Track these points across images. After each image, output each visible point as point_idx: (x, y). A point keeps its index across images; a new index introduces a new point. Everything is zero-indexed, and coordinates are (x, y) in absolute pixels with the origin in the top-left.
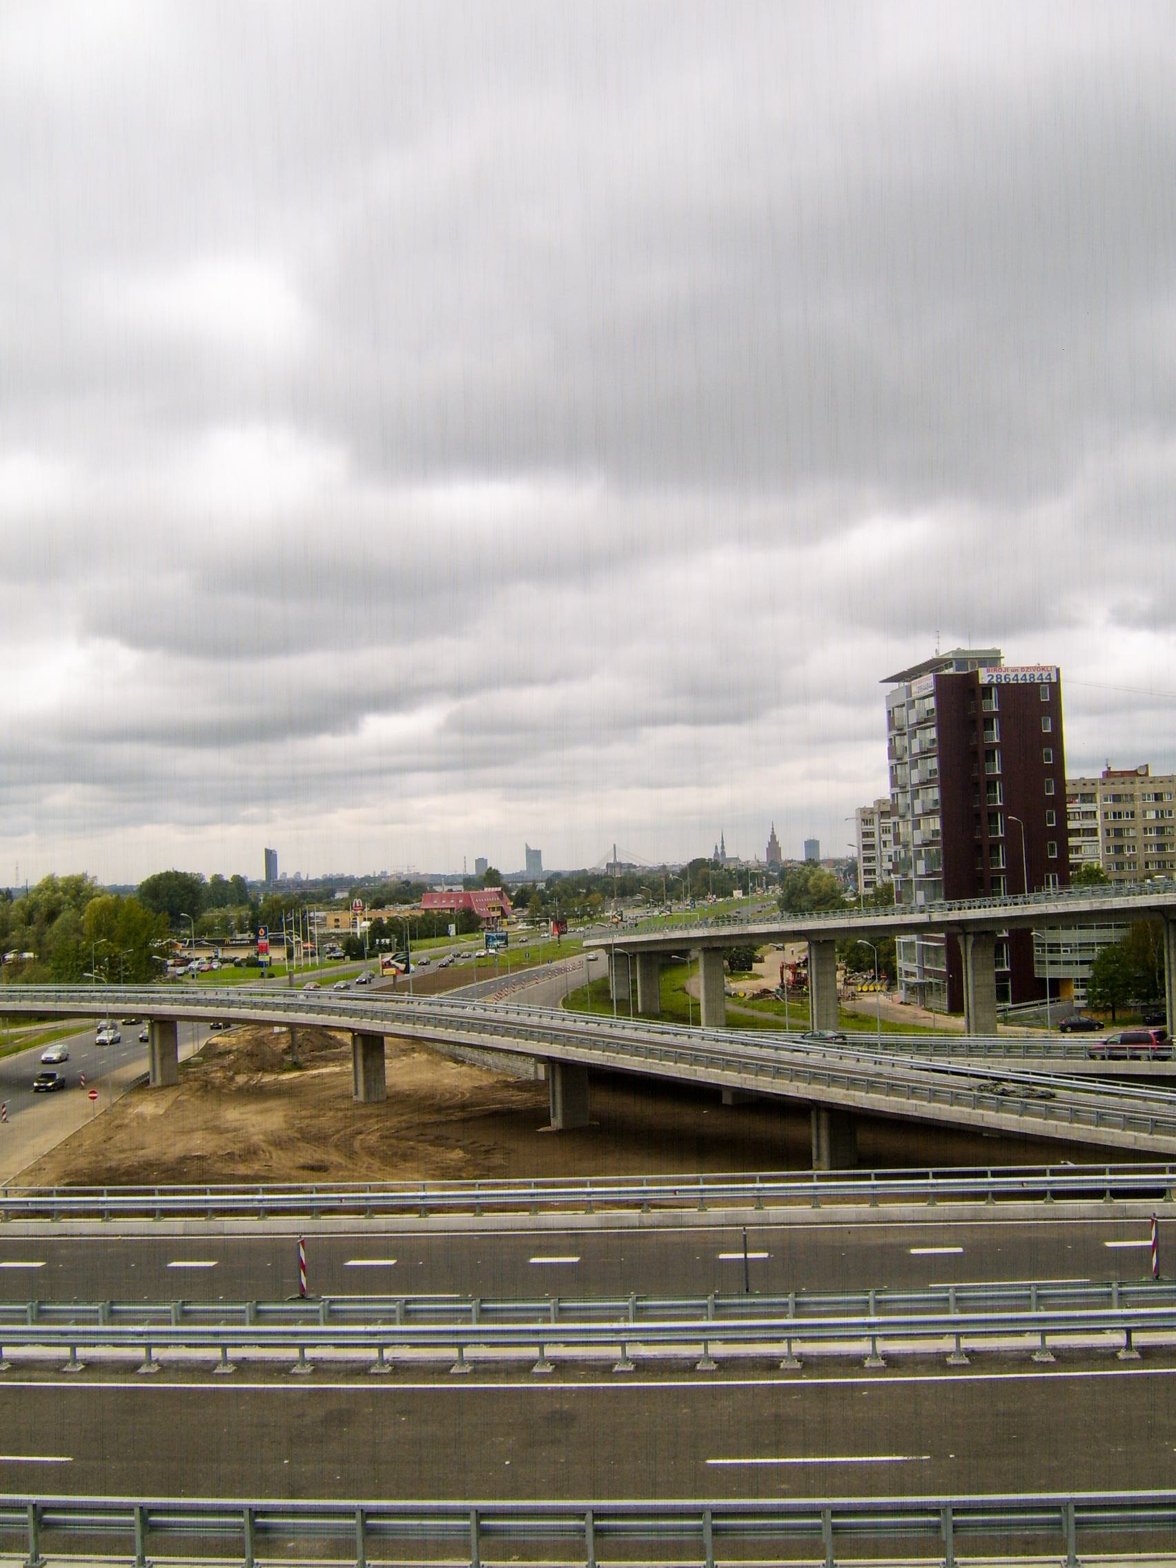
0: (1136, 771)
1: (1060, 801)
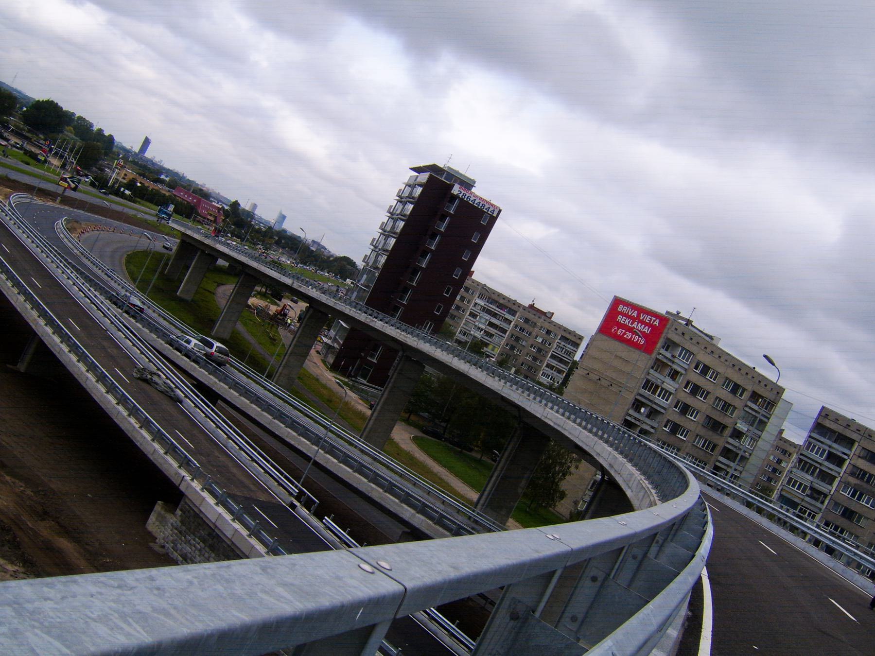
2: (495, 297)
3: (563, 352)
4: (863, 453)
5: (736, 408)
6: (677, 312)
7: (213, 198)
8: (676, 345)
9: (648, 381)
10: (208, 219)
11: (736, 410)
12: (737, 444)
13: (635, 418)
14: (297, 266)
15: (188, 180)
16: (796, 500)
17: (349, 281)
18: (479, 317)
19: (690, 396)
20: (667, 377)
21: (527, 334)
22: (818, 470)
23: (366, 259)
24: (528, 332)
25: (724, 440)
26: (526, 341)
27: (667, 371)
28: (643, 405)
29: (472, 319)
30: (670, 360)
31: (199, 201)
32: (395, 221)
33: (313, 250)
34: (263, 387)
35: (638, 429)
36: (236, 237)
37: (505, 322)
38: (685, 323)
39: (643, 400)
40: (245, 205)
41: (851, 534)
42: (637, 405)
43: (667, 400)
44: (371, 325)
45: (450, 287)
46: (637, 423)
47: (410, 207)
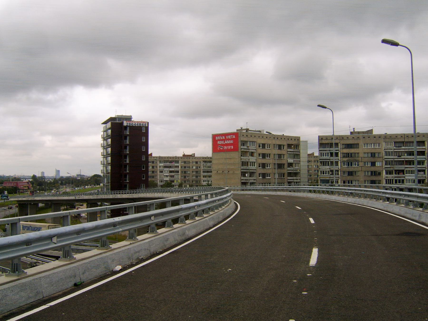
0: (191, 155)
1: (147, 162)
2: (166, 159)
3: (207, 168)
4: (344, 146)
5: (284, 155)
6: (241, 128)
7: (22, 179)
8: (246, 142)
9: (243, 162)
10: (25, 189)
11: (285, 155)
12: (292, 169)
13: (245, 180)
14: (75, 190)
15: (7, 176)
16: (327, 179)
17: (102, 185)
18: (164, 171)
19: (263, 159)
20: (249, 156)
21: (188, 168)
22: (330, 162)
23: (102, 171)
24: (188, 167)
25: (287, 170)
26: (189, 171)
27: (248, 154)
28: (246, 173)
29: (161, 173)
30: (247, 149)
31: (17, 183)
32: (106, 149)
33: (79, 179)
34: (84, 245)
35: (249, 183)
36: (42, 191)
37: (176, 168)
38: (245, 131)
39: (245, 171)
40: (38, 175)
41: (356, 181)
42: (243, 174)
43: (254, 166)
44: (116, 198)
45: (144, 165)
46: (247, 181)
47: (110, 140)
